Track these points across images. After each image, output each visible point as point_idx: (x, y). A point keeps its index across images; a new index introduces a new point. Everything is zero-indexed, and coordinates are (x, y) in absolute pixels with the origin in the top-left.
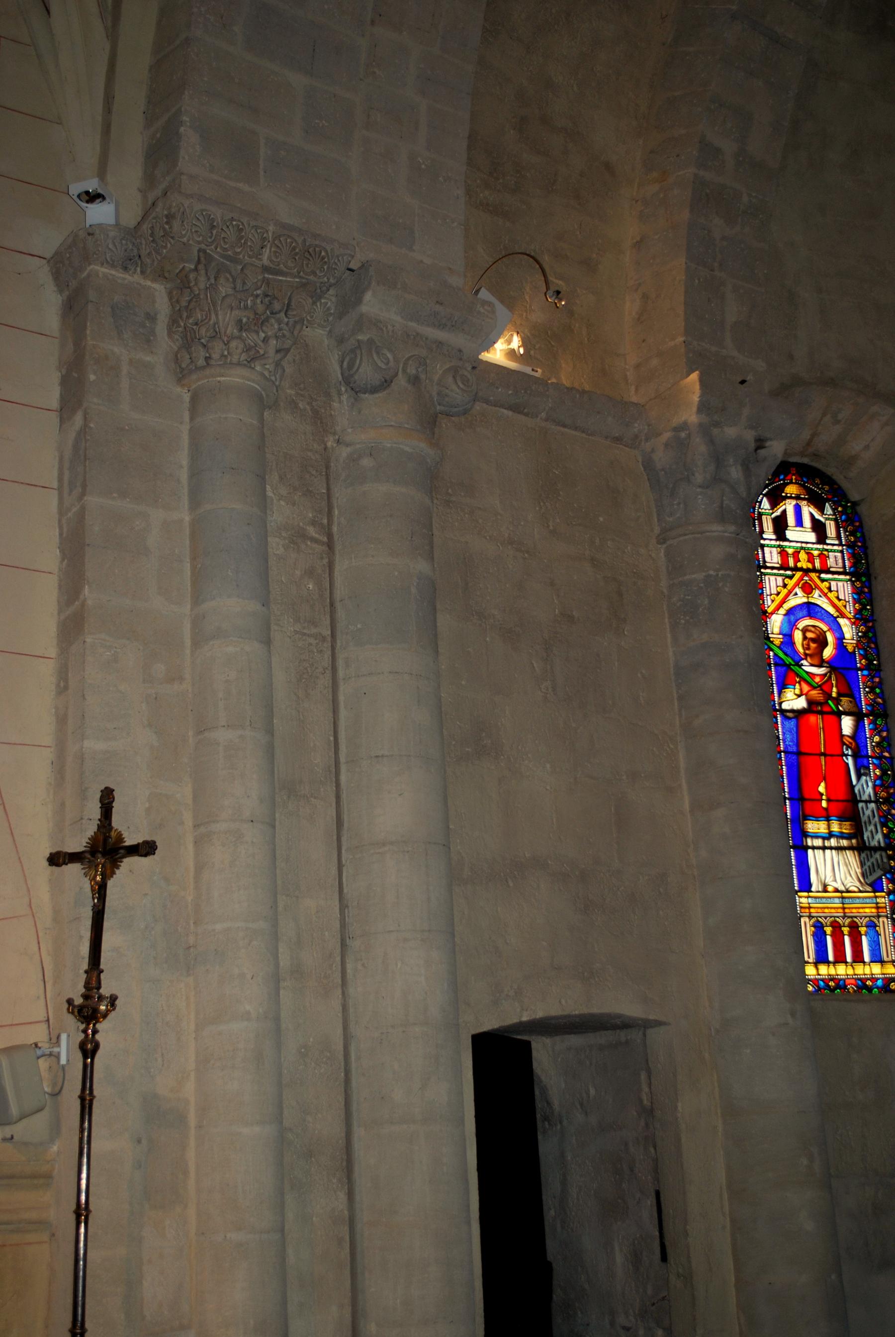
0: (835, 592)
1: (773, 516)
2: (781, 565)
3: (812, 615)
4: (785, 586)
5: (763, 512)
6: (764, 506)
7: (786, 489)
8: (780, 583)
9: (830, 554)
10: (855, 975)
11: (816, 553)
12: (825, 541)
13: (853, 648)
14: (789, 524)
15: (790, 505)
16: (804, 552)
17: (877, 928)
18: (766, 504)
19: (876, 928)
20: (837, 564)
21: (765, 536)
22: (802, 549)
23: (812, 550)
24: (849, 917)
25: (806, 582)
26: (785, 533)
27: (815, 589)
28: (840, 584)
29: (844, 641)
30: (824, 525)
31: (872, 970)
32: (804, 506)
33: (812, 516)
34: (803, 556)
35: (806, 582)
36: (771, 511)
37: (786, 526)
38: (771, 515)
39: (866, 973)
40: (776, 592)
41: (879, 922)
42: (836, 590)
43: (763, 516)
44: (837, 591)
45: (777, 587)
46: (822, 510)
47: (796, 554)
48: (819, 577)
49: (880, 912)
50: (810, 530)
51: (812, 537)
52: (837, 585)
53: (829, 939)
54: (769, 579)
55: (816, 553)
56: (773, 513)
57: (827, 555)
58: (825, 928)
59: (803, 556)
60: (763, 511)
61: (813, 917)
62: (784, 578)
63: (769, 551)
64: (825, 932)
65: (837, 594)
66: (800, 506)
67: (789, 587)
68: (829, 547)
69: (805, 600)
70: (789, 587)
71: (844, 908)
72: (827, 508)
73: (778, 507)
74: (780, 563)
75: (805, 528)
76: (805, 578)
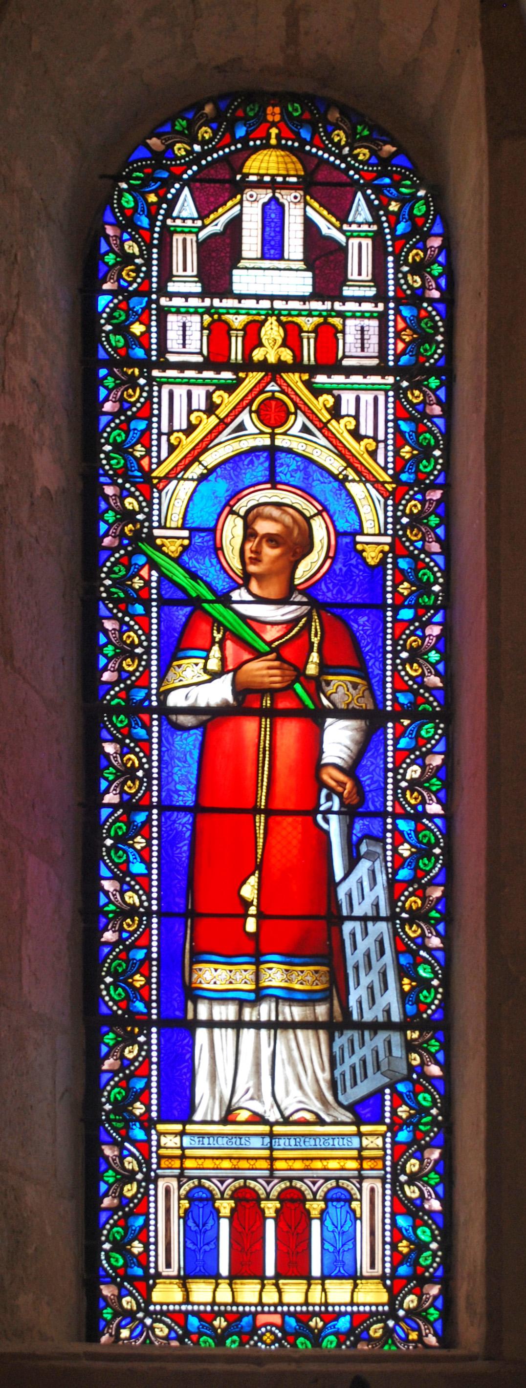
1: (203, 235)
4: (211, 408)
7: (248, 163)
8: (199, 395)
9: (349, 322)
10: (193, 1304)
11: (308, 324)
14: (245, 254)
15: (255, 204)
17: (355, 1205)
18: (186, 206)
20: (363, 349)
24: (283, 1179)
25: (273, 397)
26: (231, 276)
27: (295, 414)
28: (367, 398)
32: (292, 205)
34: (272, 332)
35: (273, 397)
36: (199, 223)
37: (235, 256)
38: (197, 234)
41: (360, 1190)
43: (175, 237)
44: (357, 417)
45: (190, 411)
46: (342, 215)
50: (301, 265)
52: (358, 399)
53: (270, 1227)
54: (171, 394)
55: (308, 324)
56: (204, 227)
57: (340, 327)
58: (263, 1204)
59: (272, 332)
60: (178, 222)
64: (308, 1212)
66: (282, 206)
67: (222, 412)
68: (351, 306)
70: (222, 412)
71: (272, 1159)
72: (359, 205)
73: (220, 210)
74: (205, 352)
76: (268, 388)
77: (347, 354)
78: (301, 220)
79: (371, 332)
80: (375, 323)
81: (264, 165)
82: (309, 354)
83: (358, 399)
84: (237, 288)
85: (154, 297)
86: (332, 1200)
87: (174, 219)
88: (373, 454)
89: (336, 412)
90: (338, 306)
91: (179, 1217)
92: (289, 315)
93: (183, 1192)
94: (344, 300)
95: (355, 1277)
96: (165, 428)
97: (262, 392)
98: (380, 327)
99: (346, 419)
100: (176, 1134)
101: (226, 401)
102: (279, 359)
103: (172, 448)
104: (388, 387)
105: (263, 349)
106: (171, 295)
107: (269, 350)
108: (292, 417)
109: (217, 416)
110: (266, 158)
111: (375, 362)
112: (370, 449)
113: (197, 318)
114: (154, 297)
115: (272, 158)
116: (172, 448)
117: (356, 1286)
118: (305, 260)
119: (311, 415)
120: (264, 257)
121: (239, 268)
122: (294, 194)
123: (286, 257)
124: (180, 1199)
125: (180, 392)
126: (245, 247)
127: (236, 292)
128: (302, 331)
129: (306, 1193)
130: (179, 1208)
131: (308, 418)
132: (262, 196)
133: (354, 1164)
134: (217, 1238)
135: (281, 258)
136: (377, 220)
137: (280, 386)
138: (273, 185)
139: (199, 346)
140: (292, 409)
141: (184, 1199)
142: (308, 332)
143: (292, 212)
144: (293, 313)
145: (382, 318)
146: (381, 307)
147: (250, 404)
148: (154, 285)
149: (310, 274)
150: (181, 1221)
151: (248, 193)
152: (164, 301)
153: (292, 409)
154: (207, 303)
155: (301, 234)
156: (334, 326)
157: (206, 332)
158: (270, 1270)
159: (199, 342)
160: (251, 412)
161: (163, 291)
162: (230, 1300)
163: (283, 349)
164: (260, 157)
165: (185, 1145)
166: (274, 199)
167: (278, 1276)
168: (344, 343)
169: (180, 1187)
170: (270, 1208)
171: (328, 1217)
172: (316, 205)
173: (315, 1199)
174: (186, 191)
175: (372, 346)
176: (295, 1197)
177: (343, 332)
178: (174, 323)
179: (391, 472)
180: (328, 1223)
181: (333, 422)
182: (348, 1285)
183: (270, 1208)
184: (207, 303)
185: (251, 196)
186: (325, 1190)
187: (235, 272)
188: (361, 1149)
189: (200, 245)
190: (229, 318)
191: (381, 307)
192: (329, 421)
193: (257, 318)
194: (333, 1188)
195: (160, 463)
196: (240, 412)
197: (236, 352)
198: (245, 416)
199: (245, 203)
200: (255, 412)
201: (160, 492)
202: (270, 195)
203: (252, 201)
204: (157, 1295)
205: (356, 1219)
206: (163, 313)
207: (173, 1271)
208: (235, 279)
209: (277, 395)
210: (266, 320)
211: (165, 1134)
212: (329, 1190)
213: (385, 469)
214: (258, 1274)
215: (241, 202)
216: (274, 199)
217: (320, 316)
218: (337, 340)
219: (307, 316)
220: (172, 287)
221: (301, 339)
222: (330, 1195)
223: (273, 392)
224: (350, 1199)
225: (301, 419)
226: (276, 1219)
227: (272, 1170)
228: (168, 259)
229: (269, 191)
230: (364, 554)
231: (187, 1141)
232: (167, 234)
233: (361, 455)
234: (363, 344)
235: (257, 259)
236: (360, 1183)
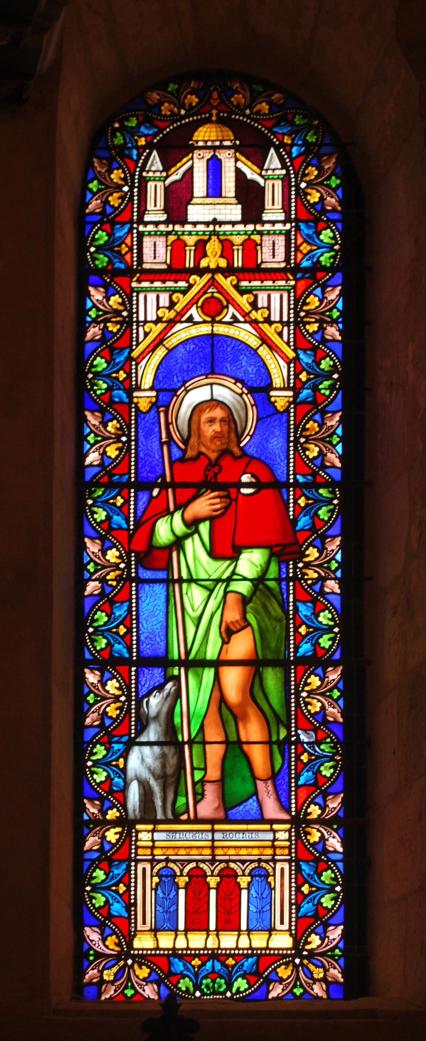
0: (265, 310)
1: (168, 182)
2: (169, 266)
3: (217, 370)
4: (172, 305)
5: (150, 177)
6: (152, 165)
7: (196, 134)
8: (164, 299)
9: (265, 238)
11: (238, 240)
12: (261, 217)
13: (287, 404)
14: (195, 195)
15: (202, 161)
16: (217, 240)
17: (271, 879)
18: (155, 162)
19: (268, 878)
20: (274, 256)
21: (147, 218)
22: (214, 235)
23: (231, 235)
24: (221, 861)
25: (212, 297)
26: (187, 210)
27: (227, 307)
28: (275, 297)
29: (272, 393)
30: (261, 190)
31: (252, 942)
32: (227, 160)
33: (239, 174)
34: (213, 247)
35: (212, 297)
36: (164, 174)
37: (189, 198)
38: (164, 181)
39: (240, 946)
40: (154, 318)
41: (274, 869)
42: (266, 305)
43: (149, 184)
44: (269, 308)
45: (158, 308)
46: (259, 162)
47: (201, 247)
48: (236, 287)
49: (277, 840)
50: (234, 201)
51: (235, 213)
52: (269, 297)
53: (213, 893)
54: (145, 298)
55: (238, 240)
56: (167, 177)
57: (259, 242)
59: (213, 247)
60: (151, 174)
61: (159, 861)
62: (171, 293)
63: (153, 243)
64: (239, 884)
65: (267, 312)
66: (220, 161)
67: (178, 307)
68: (267, 227)
69: (205, 329)
70: (178, 307)
72: (272, 158)
73: (179, 165)
74: (168, 262)
75: (225, 197)
76: (210, 291)
77: (264, 260)
78: (233, 169)
79: (280, 244)
80: (282, 238)
81: (207, 134)
82: (238, 262)
83: (269, 297)
84: (190, 218)
85: (135, 226)
86: (256, 876)
87: (148, 172)
88: (280, 334)
89: (254, 305)
90: (259, 227)
91: (152, 889)
92: (224, 234)
93: (155, 870)
94: (263, 223)
95: (271, 930)
96: (142, 318)
97: (205, 293)
98: (286, 240)
99: (262, 310)
100: (148, 831)
101: (181, 300)
102: (218, 265)
103: (146, 334)
104: (290, 288)
105: (207, 258)
106: (146, 224)
107: (212, 258)
108: (225, 311)
109: (175, 310)
110: (209, 130)
111: (283, 265)
112: (278, 331)
113: (163, 239)
114: (135, 226)
115: (212, 134)
116: (146, 334)
117: (270, 935)
118: (236, 197)
119: (238, 307)
120: (208, 196)
121: (192, 204)
122: (228, 152)
123: (223, 195)
124: (152, 876)
125: (152, 297)
126: (195, 190)
127: (189, 220)
128: (233, 245)
129: (238, 871)
130: (152, 883)
131: (235, 308)
132: (207, 154)
133: (270, 851)
134: (177, 910)
135: (219, 195)
136: (284, 166)
137: (217, 288)
138: (214, 148)
139: (165, 258)
140: (225, 303)
141: (155, 876)
142: (238, 245)
143: (227, 164)
144: (227, 233)
145: (287, 234)
146: (288, 226)
147: (197, 302)
148: (135, 218)
149: (239, 207)
150: (153, 892)
151: (196, 153)
152: (141, 228)
153: (225, 303)
154: (170, 228)
155: (233, 179)
156: (254, 241)
157: (169, 248)
158: (212, 926)
159: (165, 255)
160: (197, 307)
161: (141, 221)
162: (185, 946)
163: (220, 258)
164: (205, 129)
165: (155, 838)
166: (214, 156)
167: (218, 930)
168: (262, 253)
169: (152, 868)
170: (213, 881)
171: (253, 887)
172: (243, 159)
173: (244, 875)
174: (155, 153)
175: (280, 254)
176: (230, 874)
177: (261, 245)
178: (147, 242)
179: (292, 348)
180: (252, 892)
181: (254, 312)
182: (265, 936)
183: (213, 881)
184: (170, 228)
185: (199, 155)
186: (251, 868)
187: (190, 207)
188: (275, 840)
189: (167, 189)
190: (185, 238)
191: (288, 226)
192: (250, 312)
193: (203, 237)
194: (255, 868)
195: (138, 345)
196: (191, 307)
197: (190, 263)
198: (193, 311)
199: (196, 160)
200: (200, 307)
201: (137, 365)
202: (212, 154)
203: (200, 159)
204: (137, 944)
205: (272, 889)
206: (141, 235)
207: (147, 928)
208: (189, 212)
209: (216, 295)
210: (209, 239)
211: (141, 831)
212: (253, 869)
213: (288, 343)
214: (203, 927)
215: (192, 158)
216: (214, 156)
217: (245, 234)
218: (257, 251)
219: (237, 235)
220: (147, 218)
221: (233, 251)
222: (253, 873)
223: (213, 293)
224: (268, 875)
225: (231, 310)
226: (217, 889)
227: (213, 855)
228: (144, 194)
229: (212, 151)
230: (276, 404)
231: (157, 836)
232: (144, 182)
233: (273, 335)
234: (274, 253)
235: (203, 197)
236: (275, 864)
